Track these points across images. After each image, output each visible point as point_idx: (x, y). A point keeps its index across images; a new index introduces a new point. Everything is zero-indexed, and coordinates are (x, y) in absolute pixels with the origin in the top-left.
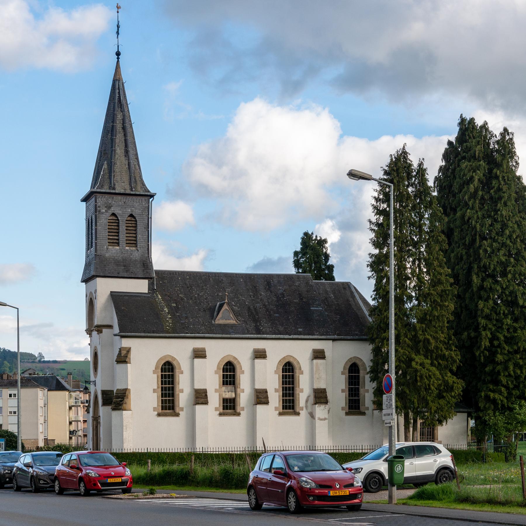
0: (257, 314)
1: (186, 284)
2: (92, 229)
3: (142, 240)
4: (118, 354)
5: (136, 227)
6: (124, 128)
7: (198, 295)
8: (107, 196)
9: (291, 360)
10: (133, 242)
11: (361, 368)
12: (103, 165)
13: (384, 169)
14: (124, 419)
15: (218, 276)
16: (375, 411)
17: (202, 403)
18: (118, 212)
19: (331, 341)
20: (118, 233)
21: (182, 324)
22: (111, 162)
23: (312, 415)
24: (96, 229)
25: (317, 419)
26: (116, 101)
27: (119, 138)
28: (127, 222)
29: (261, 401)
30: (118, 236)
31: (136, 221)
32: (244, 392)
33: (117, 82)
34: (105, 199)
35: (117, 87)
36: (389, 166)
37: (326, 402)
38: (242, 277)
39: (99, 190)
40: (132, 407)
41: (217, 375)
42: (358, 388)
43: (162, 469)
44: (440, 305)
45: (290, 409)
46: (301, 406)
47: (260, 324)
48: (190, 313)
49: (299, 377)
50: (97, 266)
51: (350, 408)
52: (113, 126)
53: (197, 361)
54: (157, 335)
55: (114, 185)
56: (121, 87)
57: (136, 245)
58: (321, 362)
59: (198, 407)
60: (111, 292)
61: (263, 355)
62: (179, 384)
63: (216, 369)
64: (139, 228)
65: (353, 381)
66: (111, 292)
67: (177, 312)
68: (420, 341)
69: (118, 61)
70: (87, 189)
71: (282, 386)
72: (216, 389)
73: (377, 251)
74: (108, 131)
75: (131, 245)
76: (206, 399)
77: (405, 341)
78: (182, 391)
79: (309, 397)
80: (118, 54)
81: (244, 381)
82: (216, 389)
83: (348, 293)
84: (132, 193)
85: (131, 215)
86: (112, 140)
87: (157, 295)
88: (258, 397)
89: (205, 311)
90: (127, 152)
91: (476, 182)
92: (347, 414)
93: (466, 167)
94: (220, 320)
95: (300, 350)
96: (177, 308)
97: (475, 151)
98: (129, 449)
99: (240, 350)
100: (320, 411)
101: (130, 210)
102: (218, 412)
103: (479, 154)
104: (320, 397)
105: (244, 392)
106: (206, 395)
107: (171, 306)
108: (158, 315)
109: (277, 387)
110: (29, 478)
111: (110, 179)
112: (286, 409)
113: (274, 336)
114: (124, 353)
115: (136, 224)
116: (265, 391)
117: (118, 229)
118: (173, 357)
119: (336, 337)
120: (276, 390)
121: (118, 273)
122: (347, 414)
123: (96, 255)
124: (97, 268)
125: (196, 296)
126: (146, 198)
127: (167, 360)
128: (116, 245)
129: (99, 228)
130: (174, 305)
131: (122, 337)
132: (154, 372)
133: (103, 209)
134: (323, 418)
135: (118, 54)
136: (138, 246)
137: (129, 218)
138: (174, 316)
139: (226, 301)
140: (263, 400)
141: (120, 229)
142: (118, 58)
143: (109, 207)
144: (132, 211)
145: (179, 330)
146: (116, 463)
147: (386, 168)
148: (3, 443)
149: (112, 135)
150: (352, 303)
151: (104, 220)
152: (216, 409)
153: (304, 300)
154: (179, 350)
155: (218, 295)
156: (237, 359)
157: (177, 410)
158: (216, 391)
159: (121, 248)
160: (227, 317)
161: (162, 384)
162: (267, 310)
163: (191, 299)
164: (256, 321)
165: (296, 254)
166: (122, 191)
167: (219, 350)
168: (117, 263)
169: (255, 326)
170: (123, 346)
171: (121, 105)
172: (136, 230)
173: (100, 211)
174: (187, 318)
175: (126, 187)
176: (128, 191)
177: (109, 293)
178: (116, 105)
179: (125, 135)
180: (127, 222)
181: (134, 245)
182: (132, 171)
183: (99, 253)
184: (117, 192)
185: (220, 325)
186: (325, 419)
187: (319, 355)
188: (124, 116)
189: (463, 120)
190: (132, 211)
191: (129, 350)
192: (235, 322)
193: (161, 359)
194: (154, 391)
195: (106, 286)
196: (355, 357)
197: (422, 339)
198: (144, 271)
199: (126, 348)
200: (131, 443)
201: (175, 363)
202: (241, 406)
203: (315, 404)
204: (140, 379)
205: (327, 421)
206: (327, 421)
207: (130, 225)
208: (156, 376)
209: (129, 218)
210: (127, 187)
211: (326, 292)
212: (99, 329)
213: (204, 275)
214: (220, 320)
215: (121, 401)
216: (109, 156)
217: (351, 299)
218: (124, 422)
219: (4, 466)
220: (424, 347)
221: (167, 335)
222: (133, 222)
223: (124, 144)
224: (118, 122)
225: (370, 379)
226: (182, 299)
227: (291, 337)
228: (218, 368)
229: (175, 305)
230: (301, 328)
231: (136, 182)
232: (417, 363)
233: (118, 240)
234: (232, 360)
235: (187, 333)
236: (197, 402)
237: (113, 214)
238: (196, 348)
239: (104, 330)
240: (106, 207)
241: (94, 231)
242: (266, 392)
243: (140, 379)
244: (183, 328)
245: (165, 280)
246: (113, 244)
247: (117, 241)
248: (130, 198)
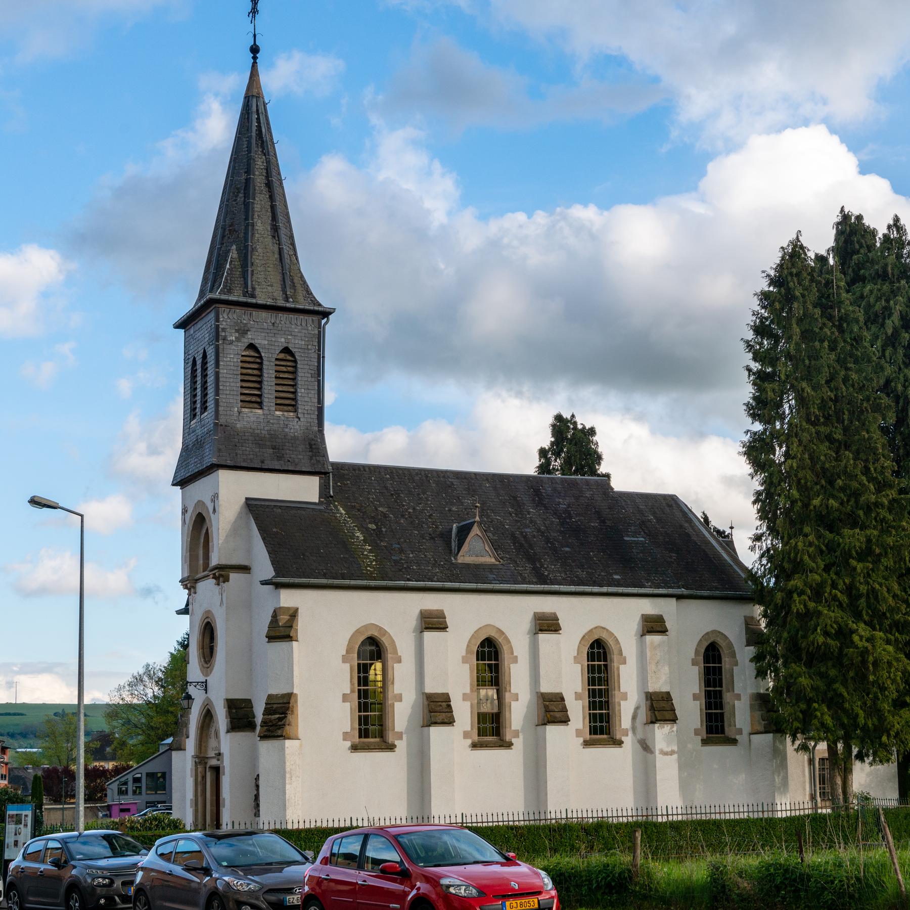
0: (531, 546)
1: (386, 488)
2: (205, 376)
3: (306, 399)
4: (271, 622)
5: (294, 373)
6: (269, 185)
7: (414, 509)
8: (238, 311)
9: (604, 636)
10: (289, 401)
12: (229, 251)
13: (768, 276)
14: (287, 757)
15: (444, 477)
16: (755, 738)
17: (443, 723)
18: (259, 341)
19: (674, 600)
20: (260, 382)
21: (396, 562)
22: (246, 247)
23: (646, 747)
24: (217, 375)
25: (657, 752)
26: (254, 134)
27: (260, 202)
28: (278, 363)
29: (555, 717)
30: (260, 389)
31: (295, 361)
32: (517, 700)
33: (255, 100)
34: (235, 316)
35: (254, 108)
36: (780, 267)
37: (674, 720)
38: (487, 479)
39: (224, 297)
41: (467, 666)
43: (706, 864)
44: (893, 527)
45: (602, 733)
46: (623, 727)
47: (542, 566)
48: (405, 541)
49: (618, 668)
50: (221, 447)
52: (247, 181)
53: (428, 636)
54: (353, 582)
55: (254, 289)
56: (261, 109)
57: (294, 407)
58: (652, 640)
59: (434, 731)
60: (247, 499)
61: (553, 625)
62: (393, 683)
63: (464, 653)
64: (300, 373)
65: (712, 677)
66: (247, 499)
67: (382, 541)
68: (860, 596)
70: (186, 304)
71: (587, 687)
72: (464, 694)
73: (758, 427)
74: (238, 189)
75: (285, 408)
76: (449, 714)
77: (836, 595)
78: (399, 698)
79: (637, 709)
80: (255, 50)
81: (518, 677)
82: (464, 694)
83: (678, 514)
84: (288, 305)
85: (286, 350)
86: (247, 207)
87: (336, 507)
88: (547, 710)
89: (432, 538)
90: (275, 229)
91: (896, 317)
92: (705, 742)
93: (871, 291)
94: (466, 557)
95: (618, 616)
96: (378, 531)
97: (886, 265)
98: (296, 821)
99: (508, 614)
101: (283, 340)
102: (469, 742)
103: (892, 269)
104: (660, 708)
105: (517, 700)
106: (449, 706)
107: (367, 529)
108: (345, 544)
109: (580, 690)
110: (63, 890)
111: (244, 275)
112: (595, 733)
113: (572, 588)
114: (283, 619)
115: (295, 367)
116: (560, 698)
117: (261, 376)
118: (381, 628)
119: (683, 591)
120: (578, 696)
121: (262, 462)
122: (705, 742)
123: (216, 424)
124: (219, 450)
125: (411, 510)
126: (315, 318)
128: (256, 405)
129: (223, 371)
130: (373, 527)
131: (279, 586)
132: (345, 659)
135: (255, 50)
136: (300, 411)
137: (282, 356)
138: (376, 548)
139: (477, 519)
140: (558, 715)
141: (265, 375)
142: (255, 58)
145: (391, 575)
146: (293, 854)
147: (772, 273)
148: (29, 813)
149: (246, 196)
150: (690, 531)
151: (233, 356)
152: (466, 735)
153: (608, 523)
154: (393, 612)
155: (450, 510)
156: (503, 633)
157: (390, 738)
158: (465, 697)
159: (266, 412)
160: (476, 551)
161: (359, 685)
162: (548, 540)
163: (403, 516)
164: (532, 559)
165: (543, 452)
166: (270, 302)
167: (471, 614)
168: (259, 441)
169: (533, 569)
170: (282, 605)
171: (263, 142)
172: (294, 379)
173: (225, 339)
174: (401, 551)
175: (275, 294)
176: (281, 303)
177: (244, 500)
178: (254, 141)
179: (272, 198)
180: (278, 363)
181: (290, 408)
182: (287, 266)
183: (222, 420)
184: (260, 302)
185: (467, 566)
186: (672, 753)
187: (654, 625)
188: (268, 162)
189: (846, 217)
191: (294, 614)
192: (493, 560)
193: (358, 632)
194: (345, 698)
195: (233, 489)
196: (714, 632)
197: (865, 591)
198: (311, 458)
199: (288, 609)
200: (300, 812)
201: (384, 640)
202: (513, 728)
203: (653, 722)
204: (317, 675)
206: (675, 756)
207: (284, 369)
208: (347, 666)
209: (282, 356)
210: (279, 294)
211: (641, 512)
212: (221, 574)
213: (417, 474)
214: (466, 557)
215: (280, 719)
216: (242, 235)
217: (686, 525)
218: (288, 764)
219: (90, 867)
220: (869, 607)
221: (373, 583)
222: (289, 364)
223: (269, 214)
224: (257, 173)
225: (755, 673)
226: (385, 516)
227: (604, 589)
228: (468, 651)
229: (374, 527)
230: (617, 574)
231: (294, 286)
232: (861, 637)
233: (260, 396)
234: (493, 634)
235: (409, 580)
236: (433, 720)
237: (251, 346)
238: (426, 611)
239: (233, 576)
240: (237, 331)
241: (211, 379)
242: (563, 699)
243: (317, 675)
244: (400, 570)
245: (347, 480)
246: (251, 405)
247: (258, 400)
248: (283, 317)
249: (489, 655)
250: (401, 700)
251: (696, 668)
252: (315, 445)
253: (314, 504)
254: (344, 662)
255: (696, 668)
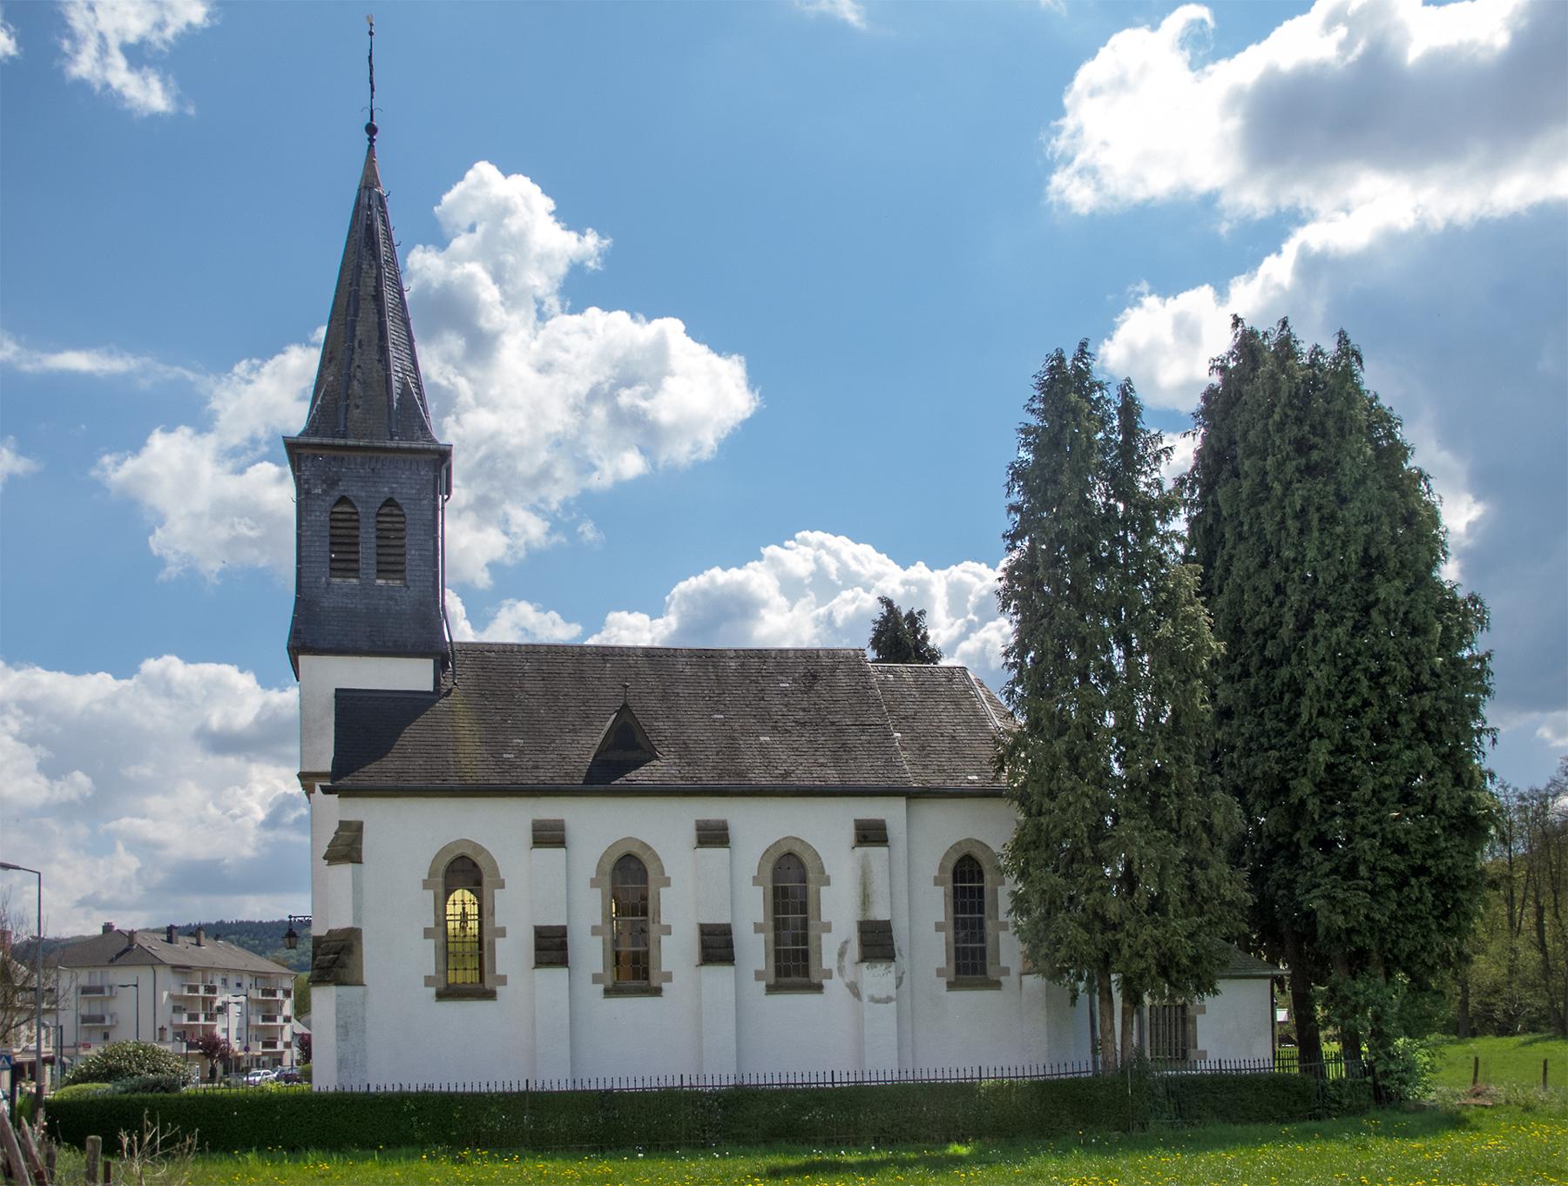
10: (390, 565)
11: (986, 868)
16: (1026, 979)
19: (902, 801)
25: (865, 999)
27: (368, 307)
40: (368, 973)
42: (981, 921)
49: (818, 892)
51: (959, 970)
62: (493, 914)
69: (371, 146)
80: (371, 130)
88: (705, 947)
100: (877, 978)
109: (761, 919)
122: (952, 986)
127: (458, 852)
133: (316, 486)
134: (884, 996)
135: (371, 130)
142: (372, 140)
143: (332, 483)
144: (392, 491)
147: (1034, 421)
186: (888, 1000)
190: (392, 491)
191: (359, 827)
205: (893, 1004)
249: (631, 881)
250: (504, 936)
251: (941, 890)
252: (431, 615)
253: (428, 693)
254: (425, 887)
255: (941, 890)
